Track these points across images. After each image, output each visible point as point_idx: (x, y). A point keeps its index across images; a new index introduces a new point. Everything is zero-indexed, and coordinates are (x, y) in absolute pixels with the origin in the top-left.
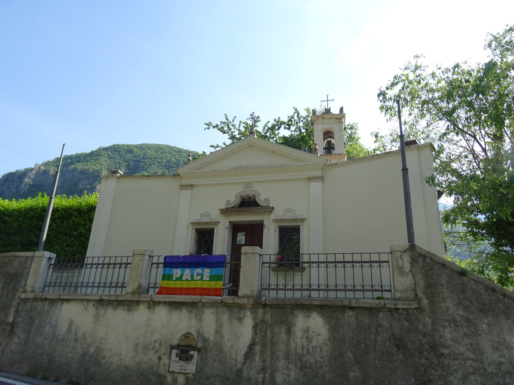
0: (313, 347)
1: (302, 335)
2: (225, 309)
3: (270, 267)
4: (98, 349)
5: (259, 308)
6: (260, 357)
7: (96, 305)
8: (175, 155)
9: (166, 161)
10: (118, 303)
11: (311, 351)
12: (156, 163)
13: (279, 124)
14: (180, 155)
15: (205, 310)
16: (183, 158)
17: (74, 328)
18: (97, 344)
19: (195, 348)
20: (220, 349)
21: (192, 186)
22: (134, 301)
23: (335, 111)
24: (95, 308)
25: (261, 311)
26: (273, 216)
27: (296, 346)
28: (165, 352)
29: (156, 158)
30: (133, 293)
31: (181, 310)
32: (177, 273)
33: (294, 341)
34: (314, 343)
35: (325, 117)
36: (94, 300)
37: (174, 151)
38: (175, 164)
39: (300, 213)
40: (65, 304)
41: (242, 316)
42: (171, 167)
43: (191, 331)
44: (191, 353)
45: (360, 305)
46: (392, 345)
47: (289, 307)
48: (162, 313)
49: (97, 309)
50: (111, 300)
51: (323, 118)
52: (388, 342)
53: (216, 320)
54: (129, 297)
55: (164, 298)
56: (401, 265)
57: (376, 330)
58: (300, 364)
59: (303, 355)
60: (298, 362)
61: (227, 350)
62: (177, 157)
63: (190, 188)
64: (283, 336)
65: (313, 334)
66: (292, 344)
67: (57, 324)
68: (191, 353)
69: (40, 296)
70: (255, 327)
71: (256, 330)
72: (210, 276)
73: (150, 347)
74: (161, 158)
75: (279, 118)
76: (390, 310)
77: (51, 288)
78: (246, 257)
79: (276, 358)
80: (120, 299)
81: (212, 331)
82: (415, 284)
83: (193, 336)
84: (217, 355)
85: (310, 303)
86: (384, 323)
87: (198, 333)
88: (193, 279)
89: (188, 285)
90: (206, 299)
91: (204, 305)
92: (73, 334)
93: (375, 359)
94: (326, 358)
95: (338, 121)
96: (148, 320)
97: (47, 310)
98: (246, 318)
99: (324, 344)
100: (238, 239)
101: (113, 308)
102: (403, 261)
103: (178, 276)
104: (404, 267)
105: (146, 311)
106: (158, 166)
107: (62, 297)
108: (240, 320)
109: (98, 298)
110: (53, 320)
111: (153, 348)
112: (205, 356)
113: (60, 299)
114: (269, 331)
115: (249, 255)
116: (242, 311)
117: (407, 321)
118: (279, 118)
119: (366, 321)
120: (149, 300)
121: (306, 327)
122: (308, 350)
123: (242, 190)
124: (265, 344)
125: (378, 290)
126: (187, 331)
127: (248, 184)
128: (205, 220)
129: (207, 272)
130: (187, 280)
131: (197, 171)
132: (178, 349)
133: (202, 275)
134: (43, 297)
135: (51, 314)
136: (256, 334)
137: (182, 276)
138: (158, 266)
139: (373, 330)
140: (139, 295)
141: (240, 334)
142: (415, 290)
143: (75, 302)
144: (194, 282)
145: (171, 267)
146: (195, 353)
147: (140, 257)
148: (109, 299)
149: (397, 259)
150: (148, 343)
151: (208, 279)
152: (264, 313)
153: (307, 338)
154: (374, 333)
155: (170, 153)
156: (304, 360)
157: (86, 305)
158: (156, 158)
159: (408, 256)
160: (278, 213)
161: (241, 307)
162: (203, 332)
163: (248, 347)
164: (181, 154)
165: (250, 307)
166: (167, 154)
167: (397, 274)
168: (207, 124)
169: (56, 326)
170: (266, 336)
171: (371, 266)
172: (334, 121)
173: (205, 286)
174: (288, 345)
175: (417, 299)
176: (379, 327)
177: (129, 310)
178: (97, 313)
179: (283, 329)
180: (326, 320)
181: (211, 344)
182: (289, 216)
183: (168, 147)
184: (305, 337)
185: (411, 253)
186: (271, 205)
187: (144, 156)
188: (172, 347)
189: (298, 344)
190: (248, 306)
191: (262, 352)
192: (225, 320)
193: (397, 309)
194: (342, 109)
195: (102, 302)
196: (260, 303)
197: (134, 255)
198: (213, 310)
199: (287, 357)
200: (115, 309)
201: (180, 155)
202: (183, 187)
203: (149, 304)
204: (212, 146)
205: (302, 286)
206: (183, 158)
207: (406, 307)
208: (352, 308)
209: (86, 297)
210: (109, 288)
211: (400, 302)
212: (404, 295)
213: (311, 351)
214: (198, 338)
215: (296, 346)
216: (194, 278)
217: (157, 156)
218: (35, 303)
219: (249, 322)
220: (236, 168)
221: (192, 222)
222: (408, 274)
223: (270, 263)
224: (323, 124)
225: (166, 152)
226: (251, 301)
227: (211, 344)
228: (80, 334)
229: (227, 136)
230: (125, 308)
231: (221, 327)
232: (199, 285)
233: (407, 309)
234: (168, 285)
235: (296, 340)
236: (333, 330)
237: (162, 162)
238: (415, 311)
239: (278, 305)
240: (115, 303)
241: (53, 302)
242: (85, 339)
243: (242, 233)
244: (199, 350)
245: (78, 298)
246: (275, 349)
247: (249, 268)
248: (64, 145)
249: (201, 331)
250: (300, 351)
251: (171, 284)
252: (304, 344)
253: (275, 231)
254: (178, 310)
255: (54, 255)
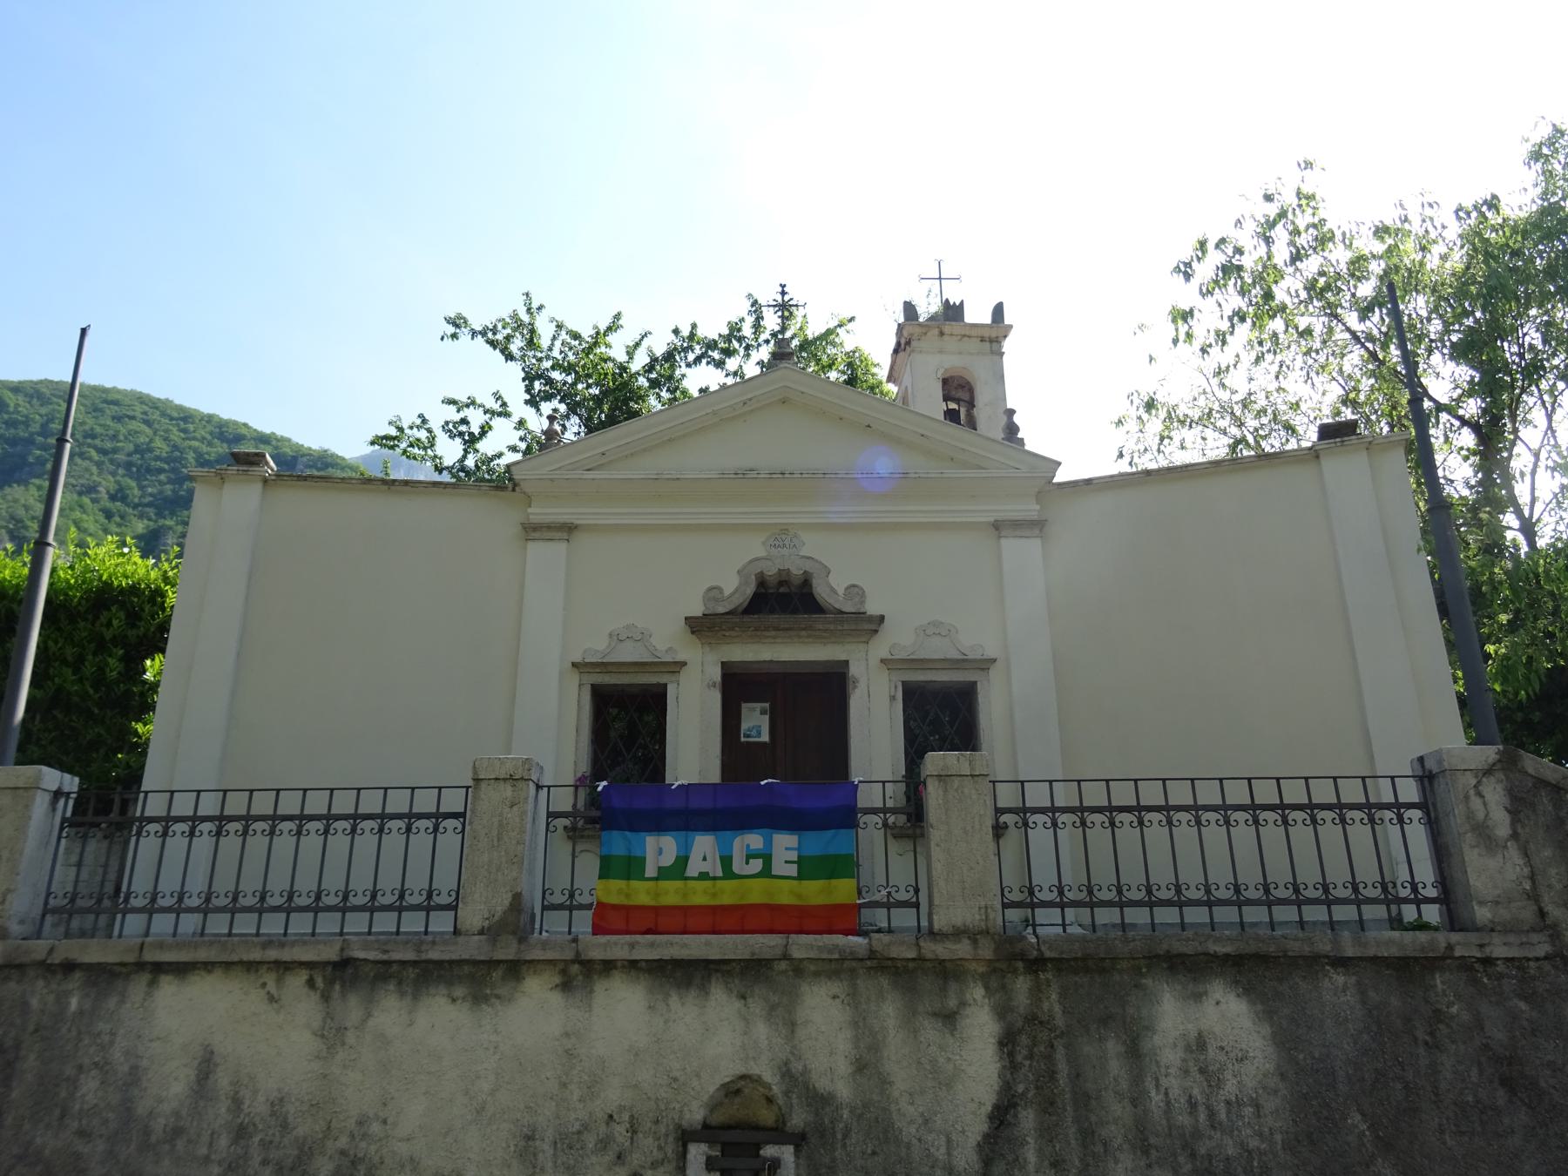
0: (1228, 1103)
1: (1184, 1060)
2: (884, 981)
3: (885, 825)
4: (354, 1163)
5: (1015, 972)
6: (1040, 1151)
7: (319, 982)
8: (167, 431)
9: (131, 447)
10: (424, 974)
11: (1223, 1116)
12: (93, 453)
13: (689, 345)
14: (185, 431)
15: (805, 988)
16: (195, 444)
17: (222, 1080)
18: (343, 1141)
19: (779, 1133)
20: (882, 1129)
21: (568, 530)
22: (499, 962)
23: (979, 314)
24: (315, 997)
25: (1021, 986)
26: (881, 647)
27: (1168, 1103)
28: (657, 1155)
29: (94, 437)
30: (492, 932)
31: (704, 990)
32: (660, 852)
33: (1157, 1086)
34: (1230, 1088)
35: (947, 329)
36: (310, 965)
37: (163, 414)
38: (167, 461)
39: (975, 638)
40: (168, 988)
41: (952, 1003)
42: (149, 470)
43: (755, 1070)
44: (769, 1151)
45: (1371, 952)
46: (1491, 1082)
47: (1124, 964)
48: (622, 1008)
49: (326, 998)
50: (387, 963)
51: (942, 334)
52: (1474, 1072)
53: (855, 1024)
54: (472, 948)
55: (632, 946)
56: (1481, 815)
57: (1432, 1034)
58: (1189, 1167)
59: (1197, 1134)
60: (1181, 1159)
61: (909, 1132)
62: (176, 436)
63: (565, 536)
64: (1116, 1067)
65: (1222, 1058)
66: (1153, 1093)
67: (134, 1069)
68: (769, 1151)
69: (40, 956)
70: (1007, 1042)
71: (1011, 1054)
72: (800, 862)
73: (590, 1141)
74: (114, 437)
75: (694, 326)
76: (1465, 965)
77: (129, 916)
78: (946, 791)
79: (1099, 1148)
80: (434, 955)
81: (843, 1067)
82: (1532, 877)
83: (768, 1087)
84: (874, 1153)
85: (1200, 949)
86: (1454, 1010)
87: (786, 1073)
88: (729, 874)
89: (657, 895)
90: (804, 945)
91: (798, 969)
92: (223, 1108)
93: (1442, 1132)
94: (1278, 1137)
95: (987, 345)
96: (567, 1035)
97: (81, 1012)
98: (968, 1011)
99: (1264, 1088)
100: (744, 726)
101: (402, 994)
102: (1485, 804)
103: (668, 859)
104: (1490, 823)
105: (556, 998)
106: (99, 464)
107: (149, 956)
108: (949, 1019)
109: (331, 953)
110: (117, 1054)
111: (604, 1143)
112: (827, 1160)
113: (140, 966)
114: (1060, 1054)
115: (956, 782)
116: (953, 987)
117: (1525, 999)
118: (694, 326)
119: (1395, 1002)
120: (569, 955)
121: (1193, 1034)
122: (1212, 1114)
123: (762, 553)
124: (1052, 1104)
125: (1109, 904)
126: (742, 1070)
127: (782, 535)
128: (628, 654)
129: (785, 845)
130: (704, 876)
131: (590, 475)
132: (711, 1142)
133: (767, 858)
134: (57, 959)
135: (102, 1026)
136: (1011, 1065)
137: (682, 861)
138: (300, 827)
139: (1421, 1034)
140: (522, 940)
141: (963, 1065)
142: (1534, 896)
143: (218, 972)
144: (735, 882)
145: (632, 829)
146: (786, 1153)
147: (507, 791)
148: (385, 957)
149: (1467, 797)
150: (577, 1126)
151: (793, 870)
152: (1037, 991)
153: (1202, 1071)
154: (1426, 1043)
155: (148, 423)
156: (1203, 1151)
157: (271, 987)
158: (94, 437)
159: (1499, 788)
160: (898, 638)
161: (947, 972)
162: (806, 1071)
163: (991, 1117)
164: (191, 427)
165: (981, 969)
166: (134, 425)
167: (1473, 847)
168: (449, 321)
169: (135, 1076)
170: (1052, 1075)
171: (1083, 823)
172: (974, 345)
173: (785, 899)
174: (1137, 1100)
175: (1546, 927)
176: (1440, 1021)
177: (478, 1000)
178: (329, 1015)
179: (1113, 1047)
180: (1259, 1007)
181: (846, 1114)
182: (937, 649)
183: (143, 399)
184: (1194, 1070)
185: (1507, 778)
186: (872, 608)
187: (44, 426)
188: (686, 1137)
189: (1175, 1093)
190: (973, 966)
191: (1047, 1133)
192: (891, 1023)
193: (1488, 961)
194: (998, 311)
195: (350, 971)
196: (1022, 956)
197: (477, 780)
198: (836, 987)
199: (1141, 1142)
200: (415, 997)
201: (185, 431)
202: (532, 530)
203: (564, 972)
204: (452, 402)
205: (572, 896)
206: (195, 444)
207: (1514, 952)
208: (1341, 962)
209: (272, 954)
210: (145, 916)
211: (1497, 939)
212: (1504, 914)
213: (1223, 1116)
214: (787, 1093)
215: (1168, 1103)
216: (736, 869)
217: (98, 430)
218: (12, 985)
219: (981, 1026)
220: (742, 474)
221: (578, 659)
222: (1505, 847)
223: (885, 810)
224: (941, 352)
225: (132, 418)
226: (987, 951)
227: (846, 1114)
228: (257, 1107)
229: (515, 371)
230: (459, 991)
231: (875, 1048)
232: (756, 893)
233: (1520, 959)
234: (685, 896)
235: (1164, 1082)
236: (1286, 1041)
237: (115, 451)
238: (1547, 966)
239: (1084, 959)
240: (411, 973)
241: (105, 977)
242: (285, 1126)
243: (758, 706)
244: (798, 1140)
245: (236, 958)
246: (1093, 1119)
247: (966, 832)
248: (84, 331)
249: (797, 1067)
250: (1183, 1119)
251: (641, 893)
252: (1196, 1092)
253: (893, 698)
254: (693, 993)
255: (71, 783)
